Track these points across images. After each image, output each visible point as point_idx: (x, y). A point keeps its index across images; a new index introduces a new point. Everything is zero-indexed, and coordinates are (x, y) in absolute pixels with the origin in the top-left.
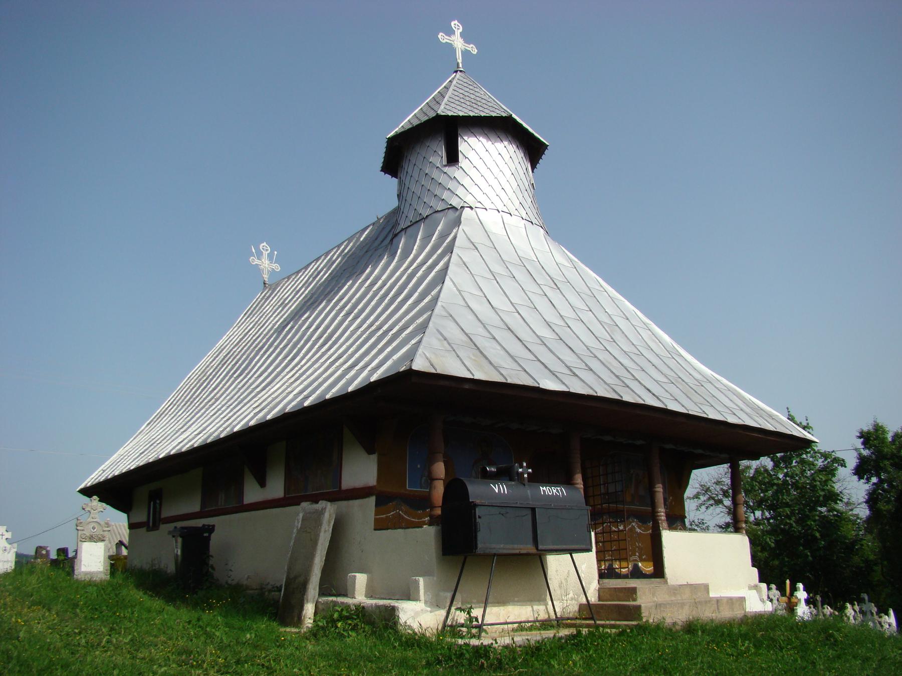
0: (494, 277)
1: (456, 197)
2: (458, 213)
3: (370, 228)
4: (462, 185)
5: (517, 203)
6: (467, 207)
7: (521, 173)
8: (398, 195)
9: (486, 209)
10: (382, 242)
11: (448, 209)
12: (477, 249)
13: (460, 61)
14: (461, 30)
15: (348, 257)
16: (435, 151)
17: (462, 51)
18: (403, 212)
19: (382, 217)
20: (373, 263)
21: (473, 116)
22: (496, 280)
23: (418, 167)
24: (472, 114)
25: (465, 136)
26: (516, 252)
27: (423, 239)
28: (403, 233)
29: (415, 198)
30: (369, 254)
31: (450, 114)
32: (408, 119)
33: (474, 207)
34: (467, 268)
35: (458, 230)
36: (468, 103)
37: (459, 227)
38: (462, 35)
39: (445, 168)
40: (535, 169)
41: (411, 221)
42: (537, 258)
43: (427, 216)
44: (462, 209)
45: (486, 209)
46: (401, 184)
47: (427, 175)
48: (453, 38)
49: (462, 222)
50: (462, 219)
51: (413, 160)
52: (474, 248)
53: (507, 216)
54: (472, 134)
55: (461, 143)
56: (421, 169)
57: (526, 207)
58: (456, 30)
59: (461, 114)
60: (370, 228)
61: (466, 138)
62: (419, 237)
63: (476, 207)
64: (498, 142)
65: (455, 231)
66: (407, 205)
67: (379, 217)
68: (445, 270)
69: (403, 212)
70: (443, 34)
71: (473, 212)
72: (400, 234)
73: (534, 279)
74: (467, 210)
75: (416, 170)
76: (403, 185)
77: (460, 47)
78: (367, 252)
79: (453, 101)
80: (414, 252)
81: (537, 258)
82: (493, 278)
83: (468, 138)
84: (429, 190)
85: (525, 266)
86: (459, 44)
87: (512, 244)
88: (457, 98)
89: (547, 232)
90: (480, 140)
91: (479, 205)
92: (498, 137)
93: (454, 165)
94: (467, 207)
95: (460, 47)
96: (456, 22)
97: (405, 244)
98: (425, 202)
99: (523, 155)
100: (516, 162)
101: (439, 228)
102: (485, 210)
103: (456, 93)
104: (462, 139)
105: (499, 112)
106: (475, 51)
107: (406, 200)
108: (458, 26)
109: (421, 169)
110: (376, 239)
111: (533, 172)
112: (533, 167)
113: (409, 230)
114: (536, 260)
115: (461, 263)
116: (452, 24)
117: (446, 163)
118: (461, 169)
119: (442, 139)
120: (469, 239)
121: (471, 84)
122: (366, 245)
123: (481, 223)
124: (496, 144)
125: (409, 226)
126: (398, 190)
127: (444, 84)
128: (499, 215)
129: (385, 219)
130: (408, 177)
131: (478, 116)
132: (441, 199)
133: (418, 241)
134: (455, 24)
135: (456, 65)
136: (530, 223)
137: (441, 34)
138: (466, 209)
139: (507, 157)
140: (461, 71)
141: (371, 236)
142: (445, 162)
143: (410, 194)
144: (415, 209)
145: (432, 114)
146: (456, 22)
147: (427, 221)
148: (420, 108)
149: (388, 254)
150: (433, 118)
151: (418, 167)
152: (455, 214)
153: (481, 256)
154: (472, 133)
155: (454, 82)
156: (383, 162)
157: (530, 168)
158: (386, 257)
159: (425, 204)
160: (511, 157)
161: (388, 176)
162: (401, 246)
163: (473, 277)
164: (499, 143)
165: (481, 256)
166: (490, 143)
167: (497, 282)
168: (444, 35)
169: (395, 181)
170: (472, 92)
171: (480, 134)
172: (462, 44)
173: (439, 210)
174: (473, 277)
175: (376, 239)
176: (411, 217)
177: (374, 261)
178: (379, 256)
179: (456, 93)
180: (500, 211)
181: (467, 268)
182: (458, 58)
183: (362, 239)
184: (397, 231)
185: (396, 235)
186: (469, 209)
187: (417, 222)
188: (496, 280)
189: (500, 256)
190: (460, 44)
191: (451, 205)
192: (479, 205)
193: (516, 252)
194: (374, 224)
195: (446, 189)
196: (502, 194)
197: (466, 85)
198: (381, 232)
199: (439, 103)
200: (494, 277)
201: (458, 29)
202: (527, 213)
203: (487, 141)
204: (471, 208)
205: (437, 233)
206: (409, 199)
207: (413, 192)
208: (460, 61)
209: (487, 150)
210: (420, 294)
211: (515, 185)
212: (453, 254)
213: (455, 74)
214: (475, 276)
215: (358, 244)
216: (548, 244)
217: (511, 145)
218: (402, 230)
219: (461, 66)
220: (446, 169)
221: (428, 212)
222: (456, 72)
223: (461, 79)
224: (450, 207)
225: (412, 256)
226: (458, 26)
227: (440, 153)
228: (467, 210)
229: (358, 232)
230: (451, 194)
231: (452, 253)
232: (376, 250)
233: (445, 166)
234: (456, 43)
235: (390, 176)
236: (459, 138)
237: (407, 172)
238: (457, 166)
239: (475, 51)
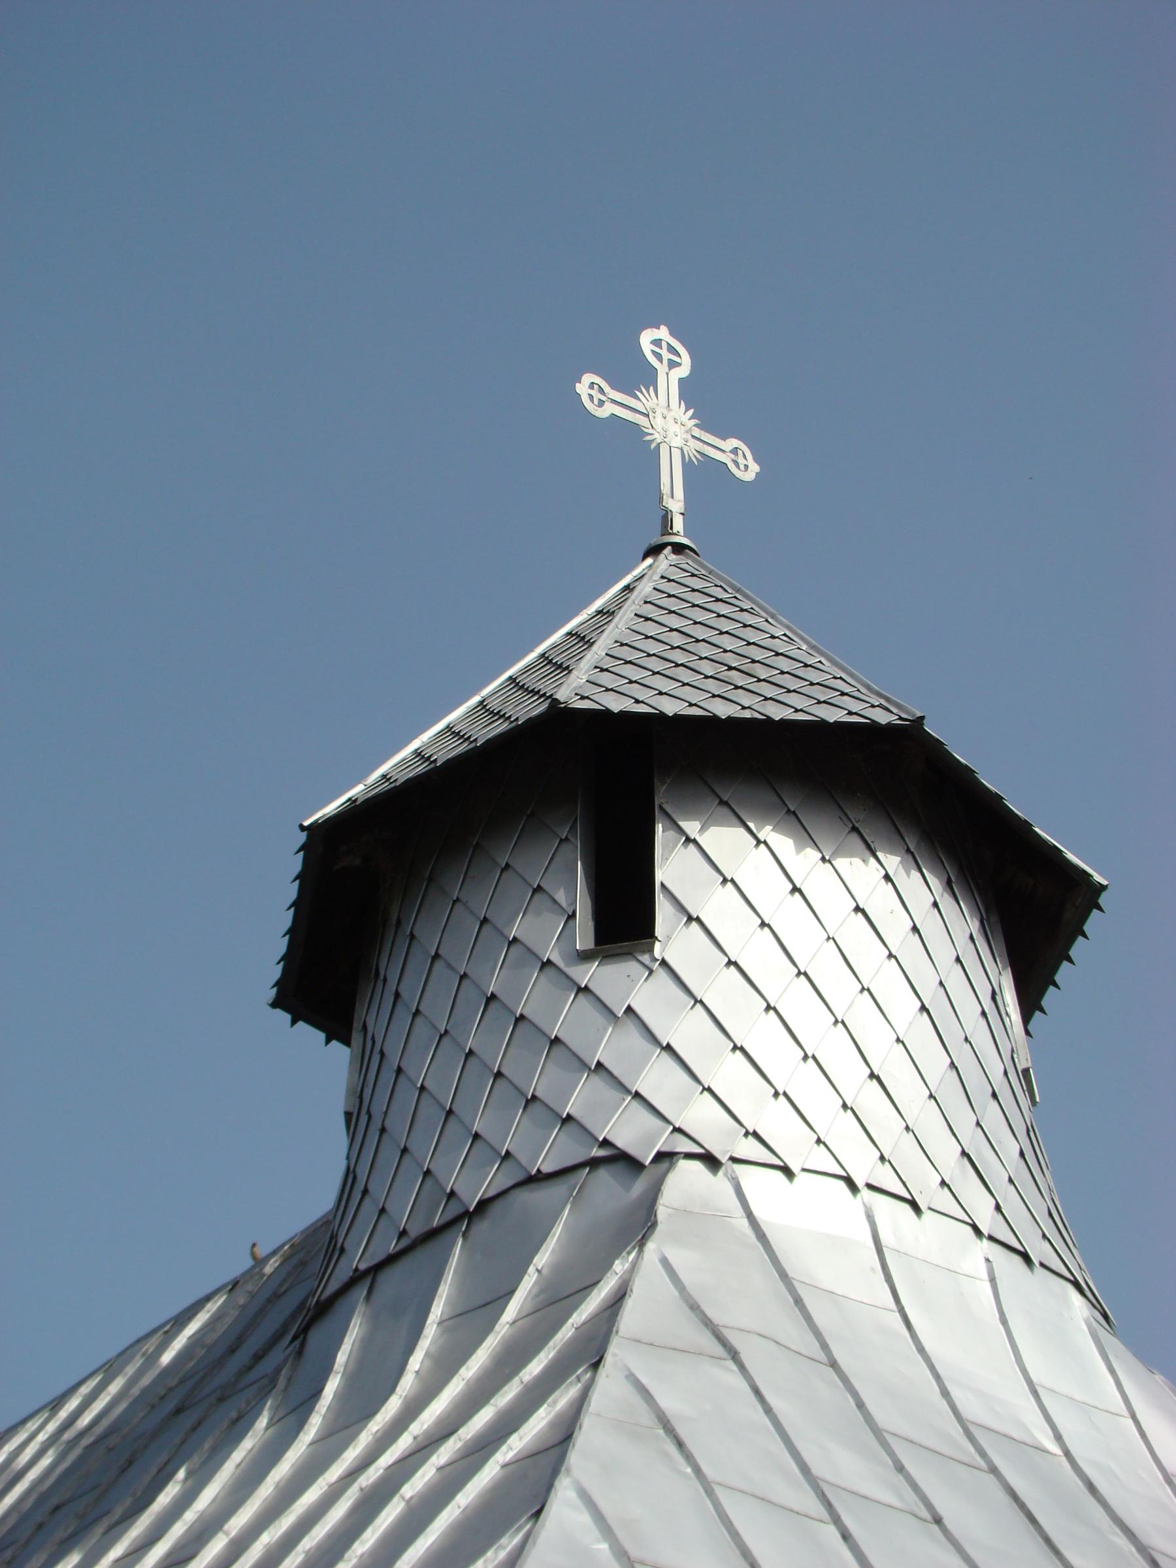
0: (829, 1506)
1: (636, 1106)
2: (640, 1185)
3: (212, 1307)
4: (669, 1048)
5: (947, 1152)
6: (689, 1156)
7: (969, 1009)
8: (348, 1115)
9: (787, 1171)
10: (258, 1357)
11: (594, 1163)
12: (734, 1355)
13: (676, 505)
14: (684, 371)
15: (86, 1448)
16: (539, 889)
17: (687, 466)
18: (365, 1192)
19: (274, 1253)
20: (196, 1459)
21: (730, 719)
22: (837, 1520)
23: (450, 966)
24: (723, 710)
25: (690, 816)
26: (945, 1393)
27: (451, 1322)
28: (361, 1291)
29: (430, 1113)
30: (189, 1419)
31: (616, 705)
32: (415, 744)
33: (724, 1159)
34: (680, 1444)
35: (634, 1265)
36: (708, 668)
37: (642, 1244)
38: (689, 391)
39: (583, 967)
40: (1038, 1014)
41: (403, 1233)
42: (1058, 1438)
43: (483, 1204)
44: (664, 1165)
45: (787, 1171)
46: (362, 1064)
47: (493, 1006)
48: (645, 400)
49: (660, 1228)
50: (662, 1212)
51: (429, 941)
52: (719, 1350)
53: (892, 1215)
54: (724, 810)
55: (670, 849)
56: (464, 976)
57: (997, 1175)
58: (662, 369)
59: (670, 708)
60: (212, 1307)
61: (691, 827)
62: (437, 1310)
63: (734, 1160)
64: (851, 855)
65: (620, 1266)
66: (389, 1154)
67: (261, 1252)
68: (555, 1452)
69: (365, 1192)
70: (597, 380)
71: (719, 1184)
72: (341, 1306)
73: (1048, 1540)
74: (689, 1172)
75: (443, 982)
76: (376, 1058)
77: (677, 442)
78: (178, 1411)
79: (633, 656)
80: (407, 1383)
81: (1058, 1438)
82: (819, 1510)
83: (702, 830)
84: (499, 1075)
85: (994, 1470)
86: (673, 428)
87: (921, 1350)
88: (653, 647)
89: (1105, 1316)
90: (761, 836)
91: (749, 1149)
92: (855, 829)
93: (629, 954)
94: (689, 1156)
95: (677, 442)
96: (663, 333)
97: (366, 1345)
98: (476, 1136)
99: (974, 926)
100: (944, 954)
101: (543, 1259)
102: (779, 1175)
103: (651, 629)
104: (671, 834)
105: (856, 706)
106: (748, 470)
107: (383, 1130)
108: (671, 349)
109: (464, 976)
110: (233, 1350)
111: (1026, 1018)
112: (1030, 1004)
113: (390, 1279)
114: (1054, 1448)
115: (646, 1417)
116: (646, 339)
117: (590, 944)
118: (661, 975)
119: (573, 828)
120: (694, 1307)
121: (723, 596)
122: (182, 1381)
123: (761, 1236)
124: (840, 863)
125: (391, 1260)
126: (350, 1092)
127: (598, 604)
128: (853, 1206)
129: (286, 1260)
130: (403, 1019)
131: (753, 721)
132: (559, 1116)
133: (431, 1330)
134: (657, 342)
135: (659, 522)
136: (1017, 1259)
137: (588, 378)
138: (683, 1164)
139: (896, 927)
140: (679, 549)
141: (214, 1336)
142: (584, 937)
143: (406, 1097)
144: (428, 1173)
145: (529, 709)
146: (663, 333)
147: (482, 1227)
148: (476, 699)
149: (275, 1409)
150: (533, 724)
151: (450, 966)
152: (628, 1189)
153: (757, 1392)
154: (723, 803)
155: (645, 589)
156: (287, 958)
157: (1010, 997)
158: (263, 1422)
159: (479, 1144)
160: (915, 929)
161: (309, 1035)
162: (342, 1358)
163: (710, 1492)
164: (857, 861)
165: (757, 1392)
166: (812, 855)
167: (846, 1536)
168: (604, 385)
169: (340, 1053)
170: (726, 626)
171: (766, 813)
172: (689, 431)
173: (547, 1168)
174: (710, 1492)
175: (233, 1350)
176: (403, 1213)
177: (207, 1446)
178: (235, 1422)
179: (651, 629)
180: (860, 1183)
181: (680, 1444)
182: (665, 489)
183: (167, 1358)
184: (334, 1286)
185: (324, 1308)
186: (697, 1166)
187: (432, 1234)
188: (837, 1520)
189: (860, 1405)
190: (677, 428)
191: (606, 1143)
192: (749, 1149)
193: (945, 1393)
194: (235, 1284)
195: (584, 1065)
196: (870, 1099)
197: (699, 599)
198: (262, 1312)
199: (565, 669)
200: (829, 1506)
201: (673, 365)
202: (998, 1208)
203: (799, 848)
204: (711, 1161)
205: (528, 1283)
206: (398, 1125)
207: (423, 1088)
208: (676, 505)
209: (795, 890)
210: (352, 1381)
211: (935, 1063)
212: (603, 1371)
213: (649, 561)
214: (718, 1491)
215: (146, 1381)
216: (1112, 1371)
217: (915, 875)
218: (357, 1277)
219: (678, 524)
220: (587, 974)
221: (490, 1180)
222: (654, 551)
223: (677, 575)
224: (602, 1153)
225: (393, 1406)
226: (671, 349)
227: (561, 896)
228: (689, 1172)
229: (154, 1331)
230: (613, 1094)
231: (596, 1365)
232: (221, 1400)
233: (585, 957)
234: (658, 422)
235: (322, 1036)
236: (659, 828)
237: (397, 995)
238: (645, 958)
239: (748, 470)
